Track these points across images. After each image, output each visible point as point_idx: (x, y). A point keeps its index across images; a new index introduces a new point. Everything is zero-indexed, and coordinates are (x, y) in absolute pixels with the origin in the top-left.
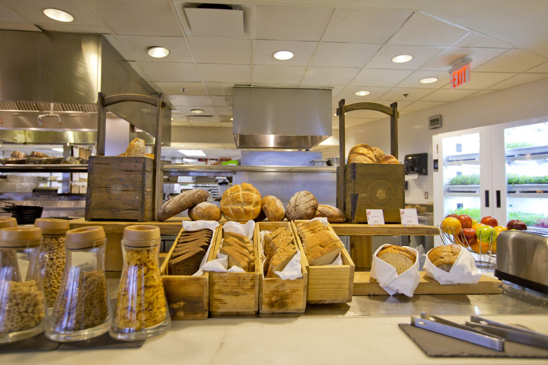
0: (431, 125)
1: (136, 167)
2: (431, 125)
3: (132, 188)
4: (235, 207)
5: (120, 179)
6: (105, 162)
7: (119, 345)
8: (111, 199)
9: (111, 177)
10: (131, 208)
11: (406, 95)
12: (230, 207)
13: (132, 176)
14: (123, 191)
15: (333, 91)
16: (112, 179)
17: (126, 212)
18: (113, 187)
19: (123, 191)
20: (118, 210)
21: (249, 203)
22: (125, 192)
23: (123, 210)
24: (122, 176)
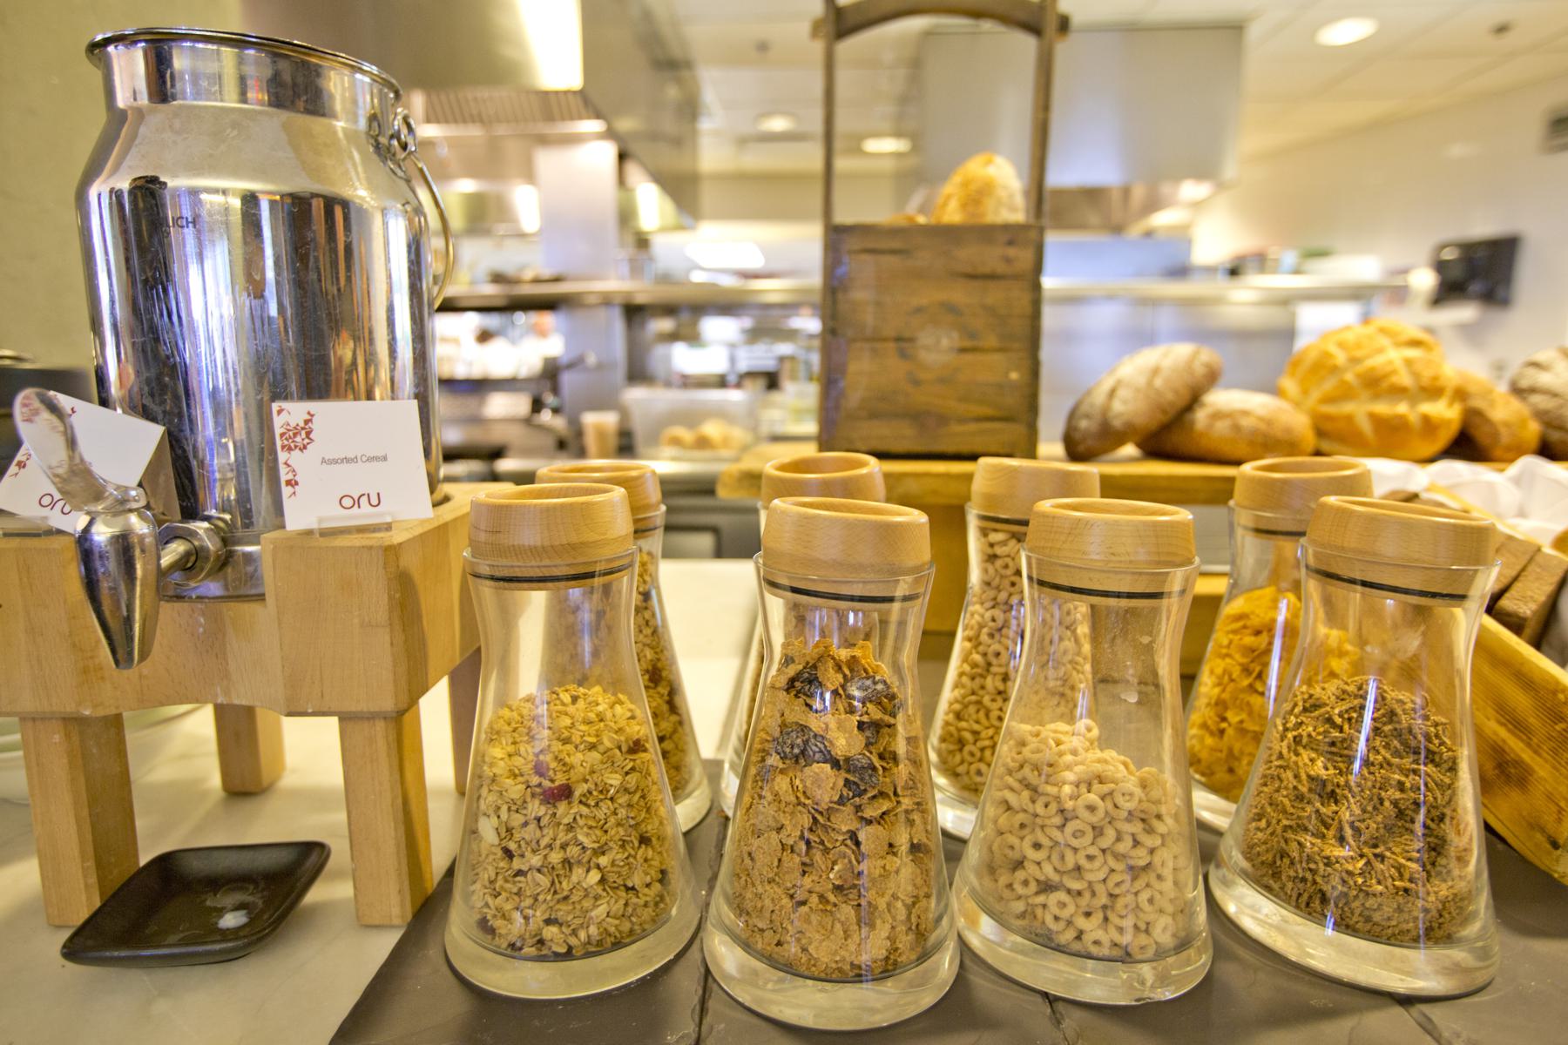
0: (370, 396)
1: (1008, 260)
2: (370, 396)
3: (992, 341)
4: (1383, 408)
5: (951, 309)
6: (896, 244)
7: (418, 828)
8: (917, 383)
9: (916, 301)
10: (990, 412)
11: (1502, 29)
12: (1360, 410)
13: (995, 295)
14: (963, 350)
15: (1254, 32)
16: (919, 310)
17: (973, 427)
18: (925, 338)
19: (963, 350)
20: (943, 419)
21: (1432, 391)
22: (969, 357)
23: (963, 420)
24: (960, 295)
